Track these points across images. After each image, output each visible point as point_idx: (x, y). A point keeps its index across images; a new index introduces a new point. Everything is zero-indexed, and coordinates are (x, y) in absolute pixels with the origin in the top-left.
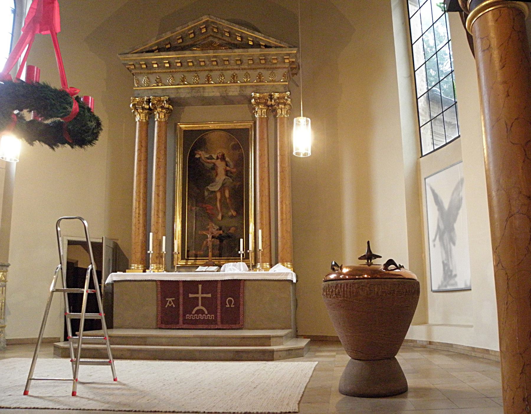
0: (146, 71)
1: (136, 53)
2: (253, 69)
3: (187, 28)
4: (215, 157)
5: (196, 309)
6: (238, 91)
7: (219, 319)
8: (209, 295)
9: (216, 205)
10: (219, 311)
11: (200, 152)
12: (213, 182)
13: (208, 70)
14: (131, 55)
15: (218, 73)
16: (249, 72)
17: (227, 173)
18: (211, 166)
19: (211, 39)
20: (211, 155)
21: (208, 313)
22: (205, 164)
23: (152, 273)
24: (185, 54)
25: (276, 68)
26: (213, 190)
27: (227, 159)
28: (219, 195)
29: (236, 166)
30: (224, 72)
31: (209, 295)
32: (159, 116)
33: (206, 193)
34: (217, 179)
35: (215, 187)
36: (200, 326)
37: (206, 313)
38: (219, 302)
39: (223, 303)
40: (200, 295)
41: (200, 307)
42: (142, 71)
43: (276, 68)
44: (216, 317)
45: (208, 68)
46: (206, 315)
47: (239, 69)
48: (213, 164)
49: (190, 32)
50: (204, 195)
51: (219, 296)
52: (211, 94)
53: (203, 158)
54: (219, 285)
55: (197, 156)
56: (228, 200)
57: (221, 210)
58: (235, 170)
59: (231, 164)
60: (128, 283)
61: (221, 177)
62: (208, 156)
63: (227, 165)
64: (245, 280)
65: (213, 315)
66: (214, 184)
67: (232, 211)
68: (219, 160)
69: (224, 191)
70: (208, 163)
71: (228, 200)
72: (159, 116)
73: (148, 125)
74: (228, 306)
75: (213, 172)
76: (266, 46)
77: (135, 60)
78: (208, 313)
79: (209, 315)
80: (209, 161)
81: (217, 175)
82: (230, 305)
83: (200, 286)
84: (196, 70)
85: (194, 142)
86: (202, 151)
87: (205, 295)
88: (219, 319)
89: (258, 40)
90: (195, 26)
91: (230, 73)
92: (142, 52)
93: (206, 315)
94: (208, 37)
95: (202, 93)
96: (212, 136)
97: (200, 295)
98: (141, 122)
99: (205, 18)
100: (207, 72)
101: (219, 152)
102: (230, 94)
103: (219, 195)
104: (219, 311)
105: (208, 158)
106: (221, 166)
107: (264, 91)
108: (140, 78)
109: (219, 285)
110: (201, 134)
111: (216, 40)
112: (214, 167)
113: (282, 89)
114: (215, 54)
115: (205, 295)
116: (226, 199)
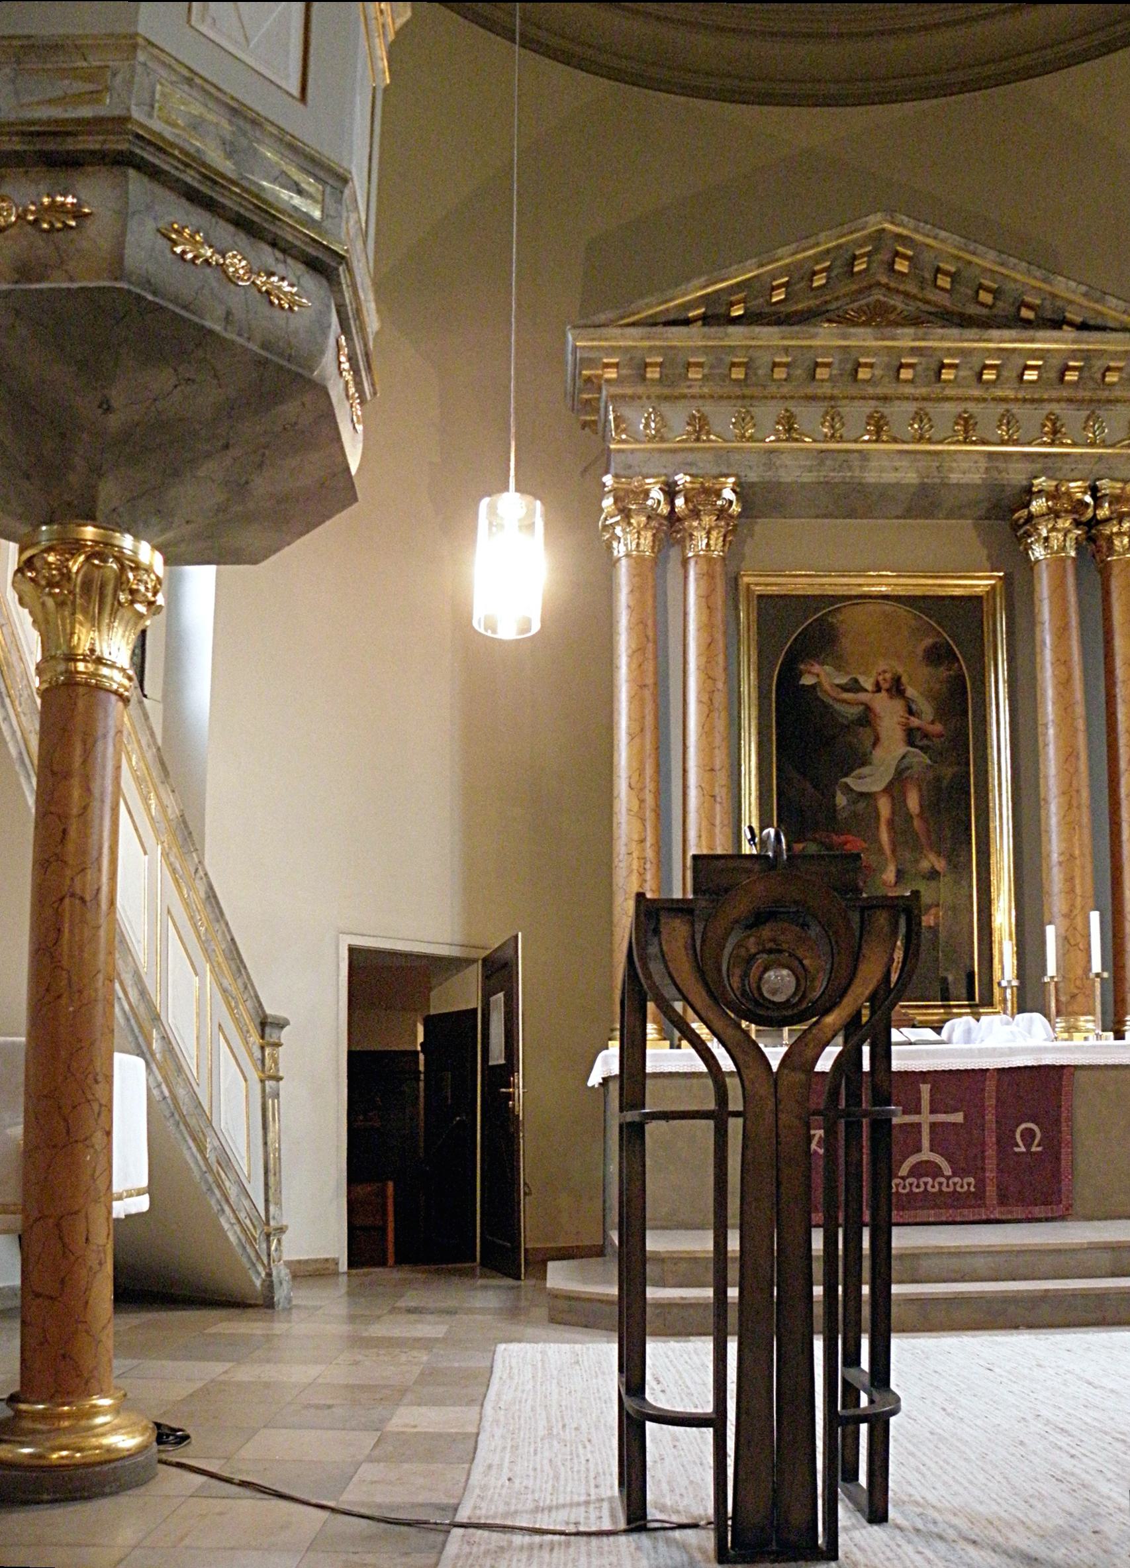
0: (657, 390)
1: (633, 324)
2: (1033, 401)
3: (811, 252)
4: (867, 683)
5: (913, 1160)
6: (982, 470)
7: (991, 1191)
8: (958, 1118)
9: (877, 840)
10: (991, 1164)
11: (816, 668)
12: (863, 764)
13: (878, 398)
14: (618, 331)
15: (912, 407)
16: (1015, 409)
17: (911, 736)
18: (853, 712)
19: (878, 295)
20: (873, 682)
21: (954, 1174)
22: (837, 706)
23: (1081, 1042)
24: (813, 337)
25: (1109, 401)
26: (864, 789)
27: (910, 692)
28: (884, 807)
29: (941, 714)
30: (930, 407)
31: (958, 1118)
32: (704, 540)
33: (841, 800)
34: (878, 753)
35: (873, 779)
36: (922, 1215)
37: (948, 1172)
38: (991, 1140)
39: (1005, 1142)
41: (926, 1155)
42: (640, 390)
43: (1109, 401)
44: (981, 1183)
45: (880, 391)
46: (948, 1178)
47: (985, 400)
48: (861, 708)
49: (818, 268)
50: (833, 808)
51: (990, 1117)
52: (890, 477)
53: (827, 687)
54: (991, 1085)
55: (807, 680)
56: (917, 823)
57: (894, 851)
58: (938, 728)
59: (927, 709)
60: (666, 1082)
61: (891, 749)
62: (843, 680)
63: (911, 712)
64: (1076, 1067)
65: (972, 1180)
66: (865, 770)
67: (932, 857)
68: (884, 694)
69: (904, 795)
70: (844, 701)
71: (917, 823)
72: (704, 540)
74: (1023, 1149)
75: (865, 734)
76: (1083, 327)
77: (627, 349)
78: (954, 1174)
79: (956, 1179)
80: (846, 696)
81: (876, 741)
82: (1028, 1146)
83: (925, 1089)
84: (836, 392)
86: (822, 664)
87: (941, 1118)
88: (991, 1191)
89: (1059, 303)
90: (839, 247)
91: (952, 408)
92: (655, 324)
93: (948, 1178)
94: (870, 287)
95: (857, 474)
96: (851, 621)
98: (638, 561)
100: (873, 403)
101: (885, 667)
103: (884, 807)
104: (991, 1164)
105: (844, 688)
106: (890, 717)
107: (1071, 475)
109: (991, 1085)
110: (817, 610)
111: (897, 302)
112: (867, 718)
114: (917, 344)
115: (941, 1118)
116: (909, 817)
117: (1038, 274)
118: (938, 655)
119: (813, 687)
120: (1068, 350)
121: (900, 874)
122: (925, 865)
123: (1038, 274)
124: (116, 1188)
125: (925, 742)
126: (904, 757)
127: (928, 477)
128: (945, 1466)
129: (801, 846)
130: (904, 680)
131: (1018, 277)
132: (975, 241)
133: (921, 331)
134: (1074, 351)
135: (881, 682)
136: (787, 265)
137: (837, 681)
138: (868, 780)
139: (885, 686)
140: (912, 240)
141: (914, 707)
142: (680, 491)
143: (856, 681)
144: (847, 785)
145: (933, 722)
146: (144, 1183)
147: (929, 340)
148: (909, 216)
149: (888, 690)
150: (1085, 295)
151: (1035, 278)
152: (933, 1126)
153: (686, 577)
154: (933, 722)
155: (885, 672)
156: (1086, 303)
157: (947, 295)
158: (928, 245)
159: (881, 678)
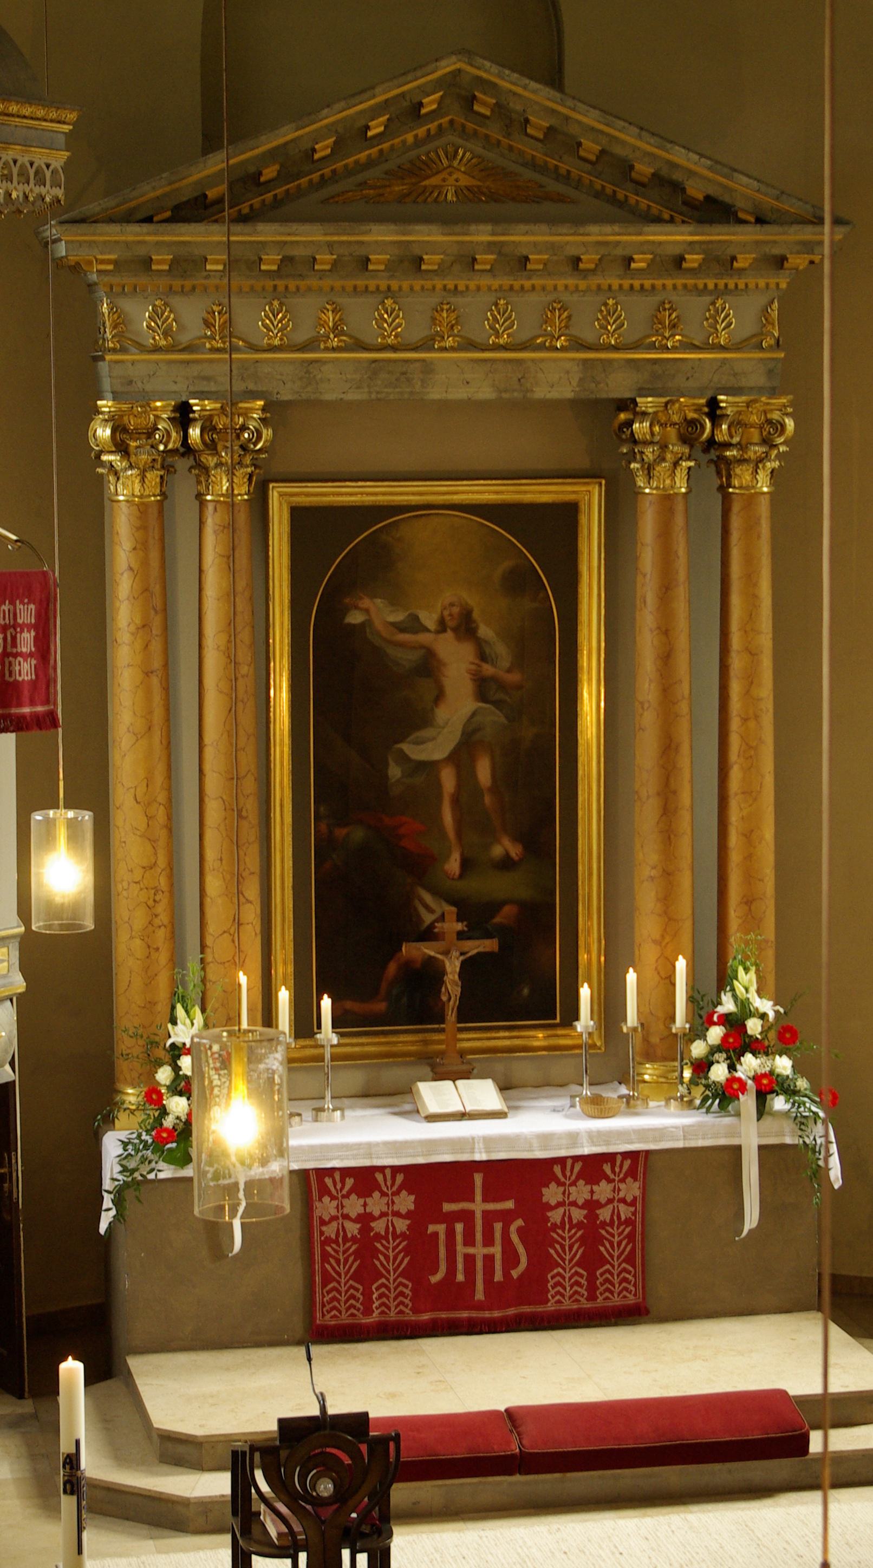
4: (429, 619)
11: (366, 603)
17: (484, 688)
18: (408, 658)
22: (390, 651)
27: (484, 631)
33: (395, 772)
34: (442, 714)
35: (435, 746)
40: (478, 1206)
48: (423, 651)
53: (378, 624)
55: (355, 618)
56: (488, 800)
59: (502, 651)
61: (458, 707)
63: (483, 657)
68: (449, 635)
69: (473, 760)
71: (488, 800)
73: (157, 519)
81: (440, 696)
83: (478, 1179)
85: (341, 558)
97: (478, 1206)
98: (142, 509)
99: (448, 66)
102: (540, 393)
105: (400, 628)
106: (457, 661)
108: (128, 305)
112: (428, 666)
113: (758, 379)
117: (652, 141)
118: (519, 582)
119: (363, 625)
120: (685, 242)
121: (466, 864)
122: (497, 851)
123: (652, 141)
124: (315, 1411)
125: (500, 696)
126: (474, 714)
127: (506, 391)
128: (615, 1550)
129: (344, 831)
130: (476, 615)
131: (627, 138)
132: (574, 98)
133: (499, 229)
134: (691, 243)
135: (448, 618)
136: (333, 124)
137: (391, 619)
138: (430, 745)
139: (450, 623)
140: (495, 85)
141: (487, 651)
142: (195, 420)
143: (416, 618)
144: (401, 751)
145: (509, 671)
146: (331, 1411)
147: (508, 235)
148: (492, 61)
149: (455, 630)
150: (710, 168)
151: (649, 144)
152: (485, 1200)
153: (202, 523)
154: (509, 671)
155: (452, 605)
156: (710, 175)
157: (540, 145)
158: (515, 94)
159: (446, 613)
